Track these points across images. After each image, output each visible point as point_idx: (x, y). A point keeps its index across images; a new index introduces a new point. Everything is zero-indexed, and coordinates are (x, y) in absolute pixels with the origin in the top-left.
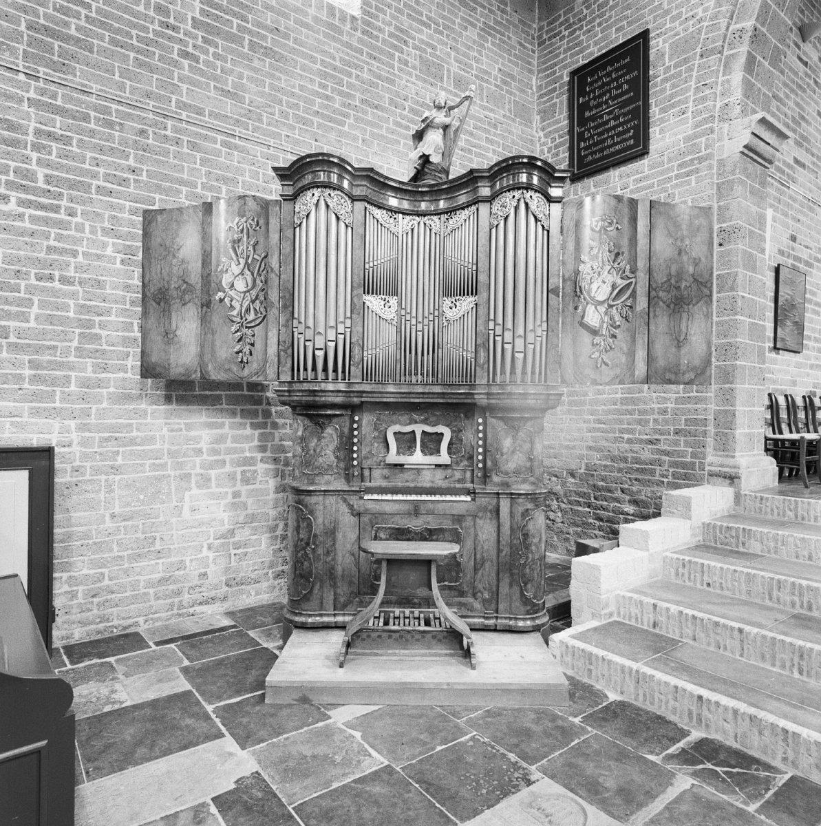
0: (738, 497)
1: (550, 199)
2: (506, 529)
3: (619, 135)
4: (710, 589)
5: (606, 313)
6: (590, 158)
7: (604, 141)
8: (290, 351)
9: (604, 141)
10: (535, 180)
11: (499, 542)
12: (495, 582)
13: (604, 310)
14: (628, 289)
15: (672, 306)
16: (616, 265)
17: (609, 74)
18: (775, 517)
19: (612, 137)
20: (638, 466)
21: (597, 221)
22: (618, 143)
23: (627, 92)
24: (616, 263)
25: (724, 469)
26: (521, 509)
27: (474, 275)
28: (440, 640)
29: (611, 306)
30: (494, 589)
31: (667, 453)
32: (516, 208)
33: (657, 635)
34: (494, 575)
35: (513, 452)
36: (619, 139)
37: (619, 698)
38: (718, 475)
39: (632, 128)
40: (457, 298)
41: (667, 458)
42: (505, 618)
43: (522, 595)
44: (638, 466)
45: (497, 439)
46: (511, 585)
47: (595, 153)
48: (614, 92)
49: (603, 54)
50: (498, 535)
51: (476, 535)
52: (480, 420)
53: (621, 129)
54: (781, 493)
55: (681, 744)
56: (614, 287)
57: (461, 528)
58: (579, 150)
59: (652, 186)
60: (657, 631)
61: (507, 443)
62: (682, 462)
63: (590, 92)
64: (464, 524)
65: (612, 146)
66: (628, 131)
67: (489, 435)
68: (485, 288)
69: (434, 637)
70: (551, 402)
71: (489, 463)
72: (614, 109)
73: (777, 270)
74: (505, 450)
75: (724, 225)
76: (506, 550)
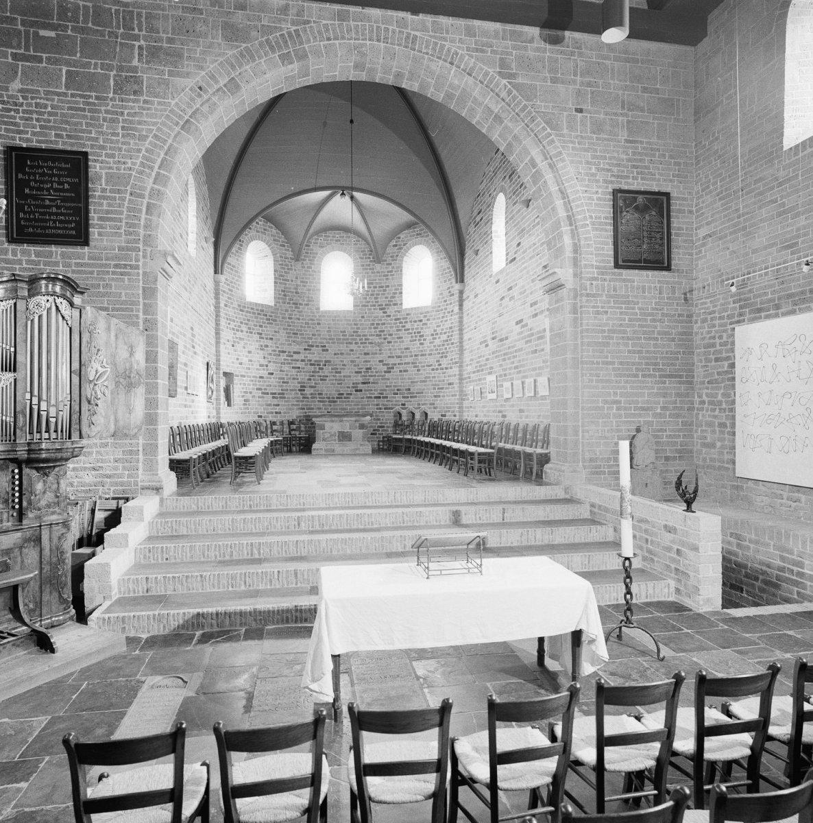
0: (162, 500)
1: (72, 304)
2: (47, 552)
3: (61, 221)
4: (168, 561)
6: (31, 230)
7: (46, 221)
9: (46, 221)
10: (58, 289)
11: (41, 562)
12: (38, 594)
17: (51, 168)
18: (186, 510)
19: (55, 222)
20: (83, 488)
22: (59, 228)
23: (66, 191)
25: (154, 484)
26: (58, 534)
27: (13, 354)
28: (18, 646)
30: (38, 599)
31: (109, 477)
32: (49, 310)
33: (151, 596)
34: (37, 588)
35: (44, 492)
36: (61, 225)
37: (148, 635)
38: (148, 488)
39: (75, 222)
41: (109, 480)
42: (48, 619)
43: (60, 596)
44: (83, 488)
45: (31, 485)
46: (51, 593)
47: (37, 227)
48: (55, 185)
49: (41, 150)
50: (41, 557)
51: (22, 562)
53: (62, 218)
54: (183, 495)
55: (195, 639)
57: (10, 559)
58: (18, 220)
59: (92, 273)
60: (150, 594)
61: (39, 486)
62: (121, 482)
63: (27, 173)
64: (12, 555)
65: (51, 228)
66: (70, 222)
67: (25, 482)
68: (23, 367)
69: (13, 645)
70: (75, 453)
71: (25, 504)
72: (56, 199)
73: (208, 364)
74: (37, 492)
75: (149, 317)
76: (46, 568)
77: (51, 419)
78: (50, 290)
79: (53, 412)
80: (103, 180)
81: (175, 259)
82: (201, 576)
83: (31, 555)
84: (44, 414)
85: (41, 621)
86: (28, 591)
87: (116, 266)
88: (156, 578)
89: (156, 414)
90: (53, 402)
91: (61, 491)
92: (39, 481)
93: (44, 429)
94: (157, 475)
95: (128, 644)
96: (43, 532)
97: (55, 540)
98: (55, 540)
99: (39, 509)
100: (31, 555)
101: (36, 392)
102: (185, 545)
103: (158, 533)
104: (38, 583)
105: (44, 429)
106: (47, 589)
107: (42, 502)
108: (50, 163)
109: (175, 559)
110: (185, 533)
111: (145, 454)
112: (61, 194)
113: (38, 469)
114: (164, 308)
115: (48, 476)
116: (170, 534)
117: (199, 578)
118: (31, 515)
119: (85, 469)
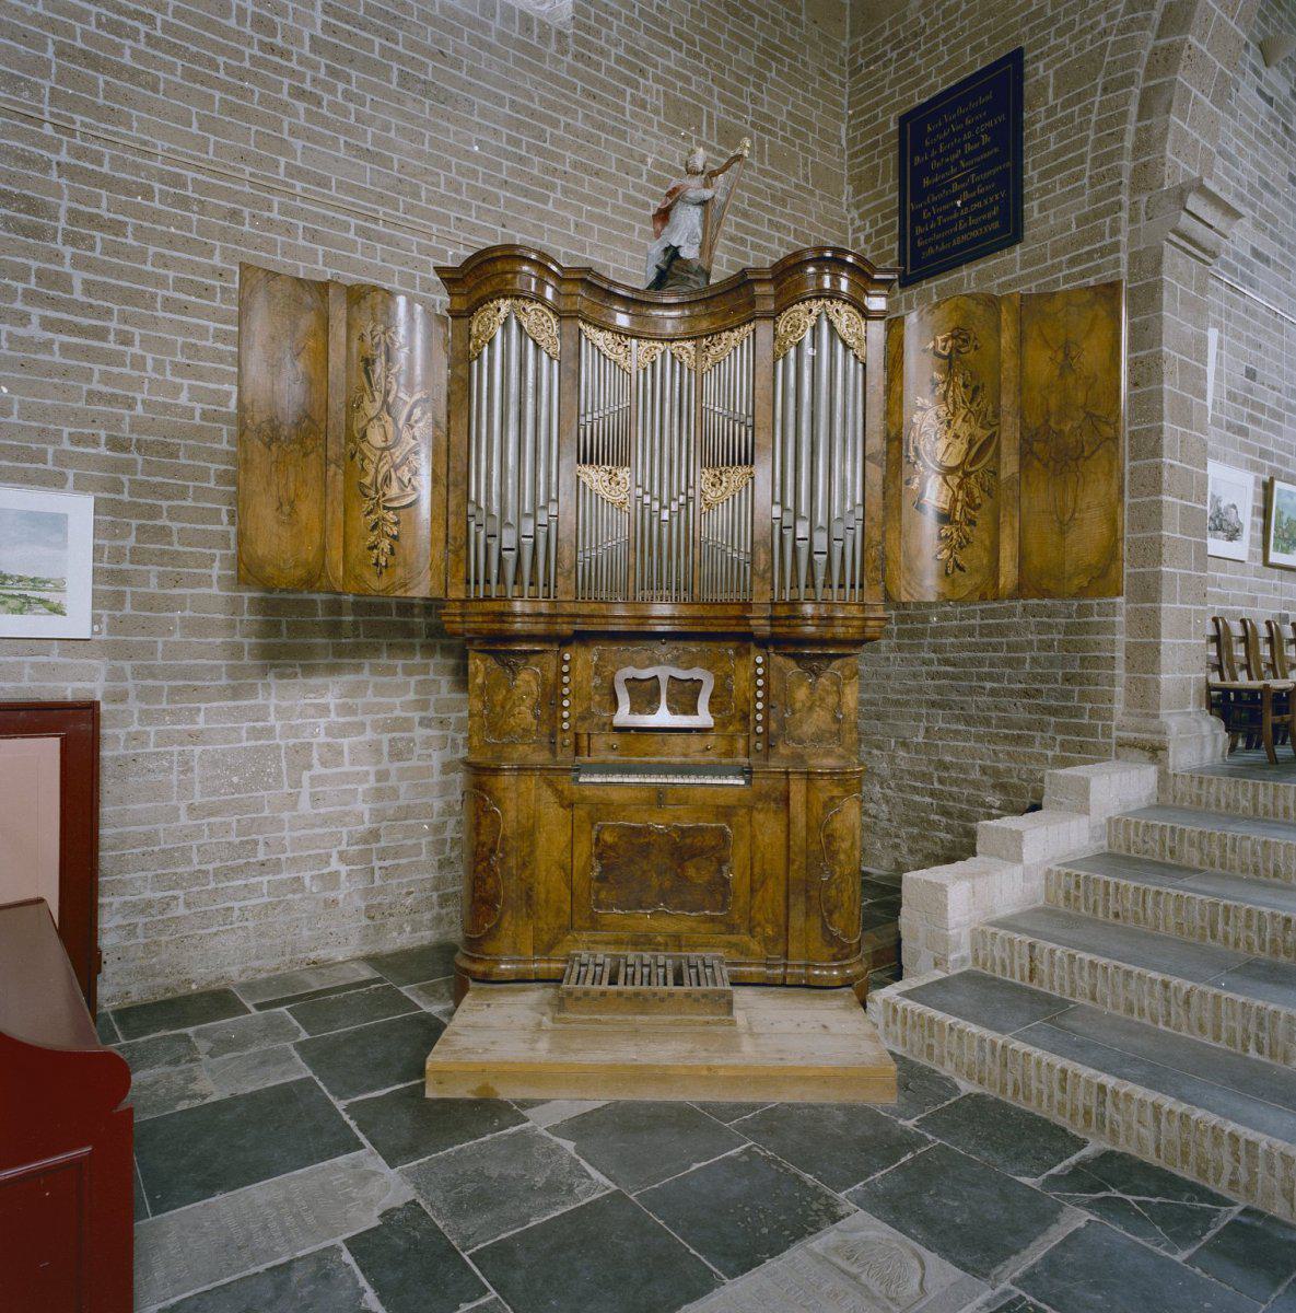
0: (1163, 776)
4: (1119, 922)
5: (960, 486)
6: (931, 251)
8: (463, 553)
10: (844, 285)
13: (957, 480)
14: (990, 443)
15: (1051, 463)
16: (974, 407)
21: (946, 340)
22: (974, 227)
24: (975, 404)
25: (1146, 736)
26: (823, 797)
29: (967, 475)
30: (782, 921)
34: (780, 898)
35: (811, 708)
37: (978, 1090)
38: (1132, 745)
39: (995, 202)
40: (723, 469)
43: (825, 929)
48: (969, 148)
52: (759, 660)
56: (971, 443)
58: (914, 239)
61: (801, 694)
67: (774, 683)
77: (816, 557)
78: (827, 285)
79: (821, 541)
80: (1051, 90)
81: (1213, 199)
82: (1166, 985)
83: (769, 828)
84: (803, 546)
85: (786, 966)
86: (764, 901)
87: (1073, 262)
88: (1052, 952)
89: (1158, 576)
90: (821, 519)
91: (845, 710)
92: (800, 686)
93: (820, 579)
94: (1156, 716)
95: (903, 1086)
96: (793, 788)
97: (817, 809)
98: (817, 809)
99: (801, 741)
100: (769, 828)
101: (804, 510)
102: (1164, 890)
103: (1129, 850)
104: (783, 888)
105: (820, 579)
106: (799, 907)
107: (805, 728)
108: (960, 111)
109: (1137, 920)
110: (1196, 863)
111: (1130, 668)
112: (978, 159)
113: (798, 658)
114: (1190, 328)
115: (818, 676)
116: (1157, 858)
117: (1158, 988)
118: (783, 750)
119: (1012, 693)
